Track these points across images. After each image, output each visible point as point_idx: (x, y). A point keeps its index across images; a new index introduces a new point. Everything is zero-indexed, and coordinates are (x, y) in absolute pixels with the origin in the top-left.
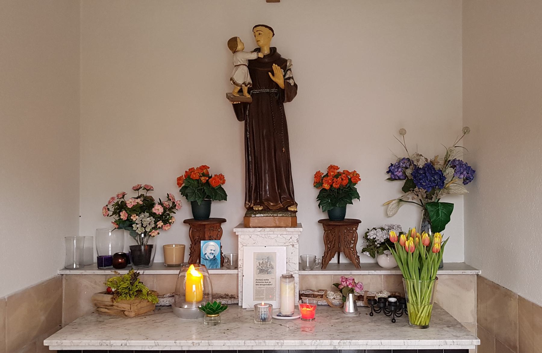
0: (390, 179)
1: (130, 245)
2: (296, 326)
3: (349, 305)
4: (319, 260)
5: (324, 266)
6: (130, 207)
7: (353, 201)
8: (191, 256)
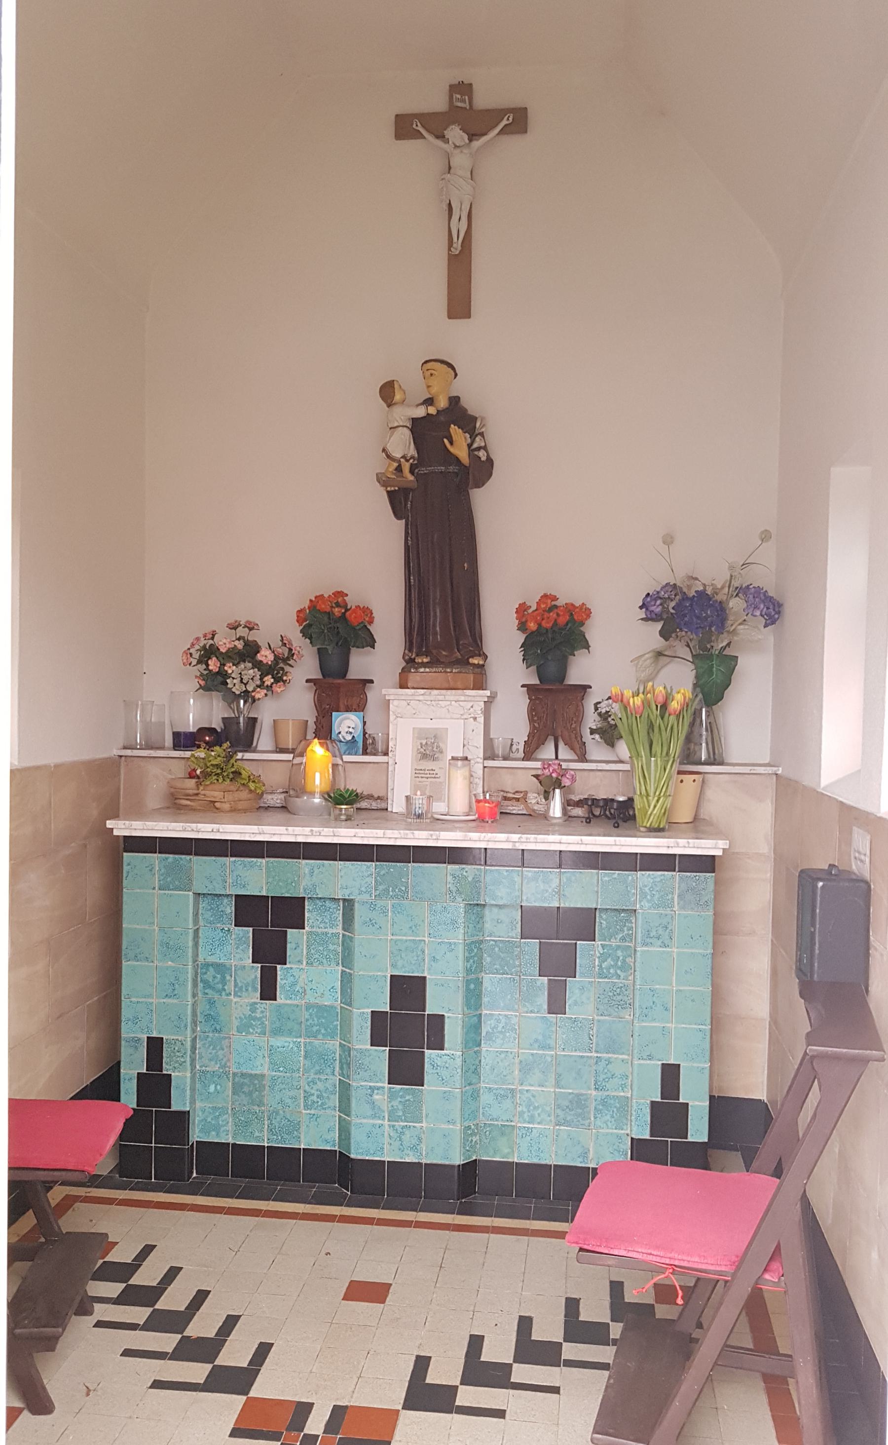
3: (554, 806)
6: (224, 651)
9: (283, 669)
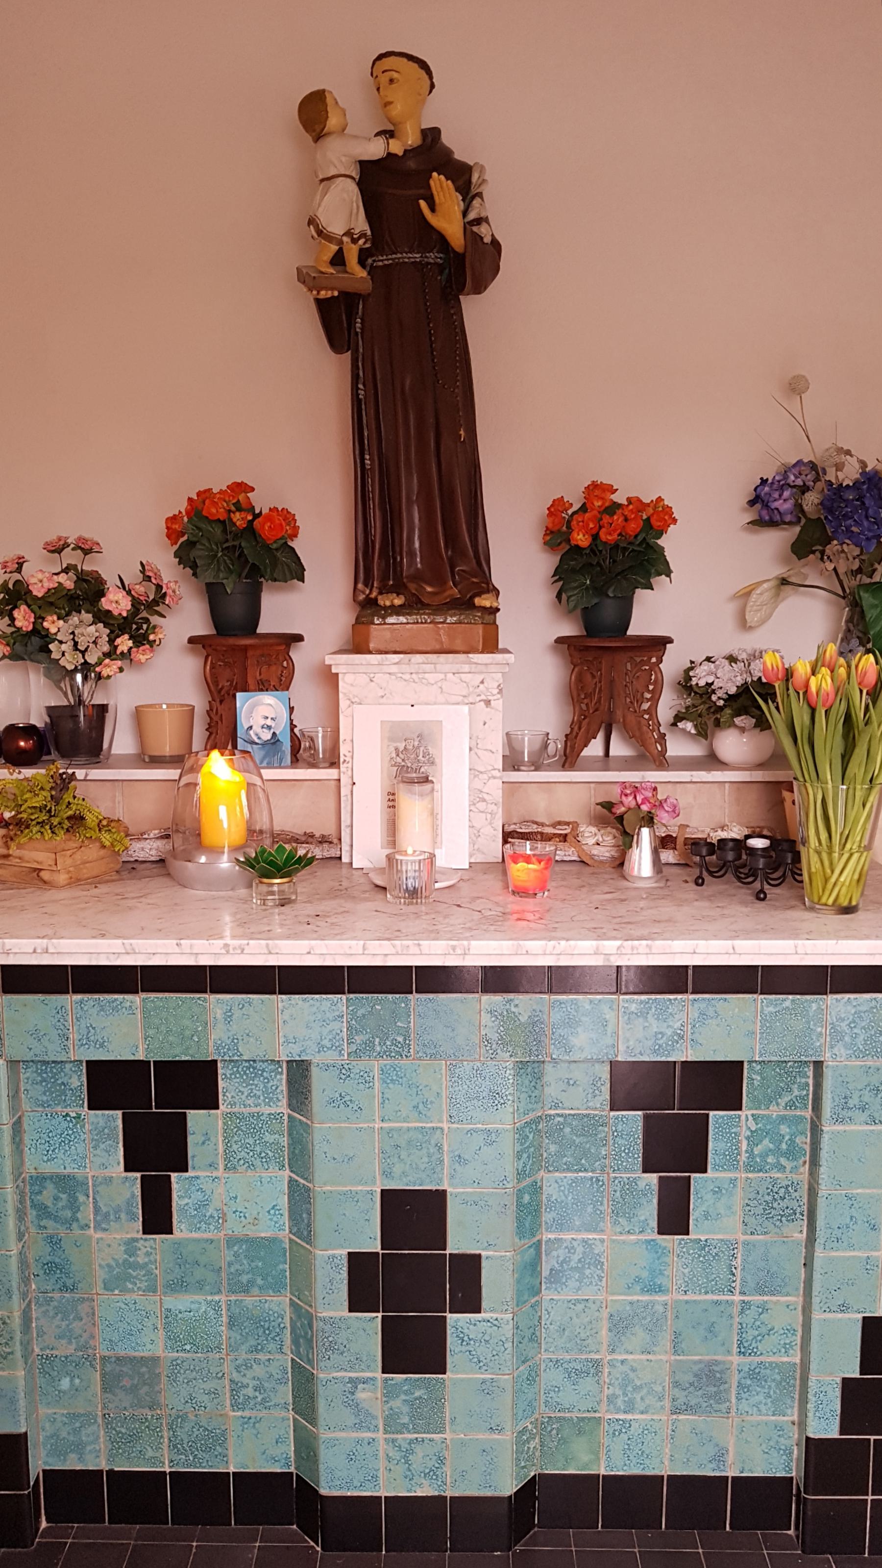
0: (759, 523)
1: (47, 705)
2: (501, 909)
4: (556, 745)
5: (569, 760)
6: (40, 595)
7: (653, 581)
8: (211, 734)
9: (147, 621)
